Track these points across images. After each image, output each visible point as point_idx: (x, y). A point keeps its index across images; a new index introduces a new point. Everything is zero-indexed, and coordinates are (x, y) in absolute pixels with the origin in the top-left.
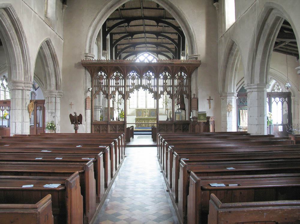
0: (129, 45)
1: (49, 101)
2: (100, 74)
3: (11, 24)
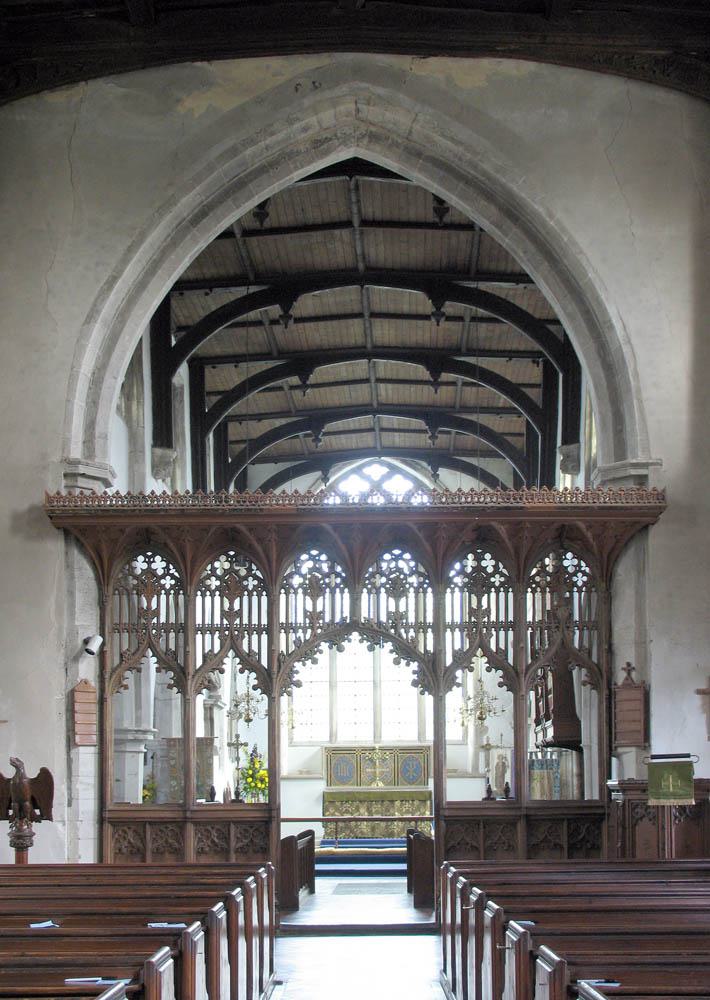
0: (289, 420)
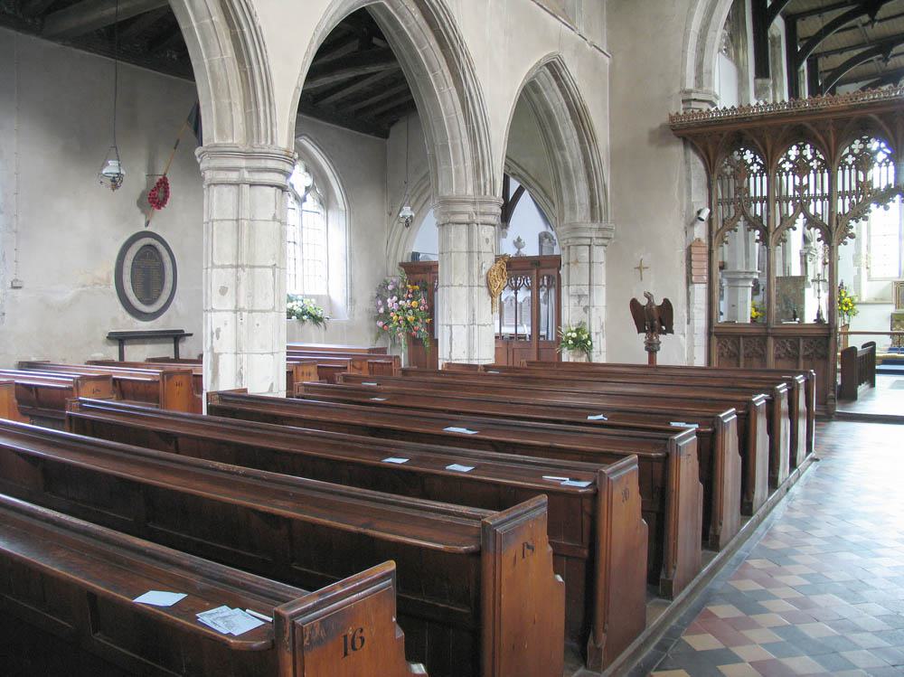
0: (865, 49)
1: (572, 260)
2: (862, 146)
3: (423, 22)
